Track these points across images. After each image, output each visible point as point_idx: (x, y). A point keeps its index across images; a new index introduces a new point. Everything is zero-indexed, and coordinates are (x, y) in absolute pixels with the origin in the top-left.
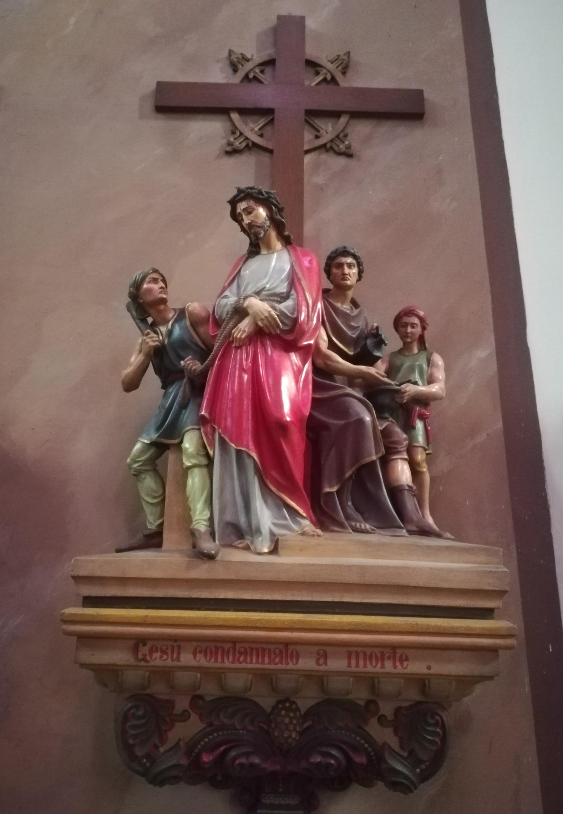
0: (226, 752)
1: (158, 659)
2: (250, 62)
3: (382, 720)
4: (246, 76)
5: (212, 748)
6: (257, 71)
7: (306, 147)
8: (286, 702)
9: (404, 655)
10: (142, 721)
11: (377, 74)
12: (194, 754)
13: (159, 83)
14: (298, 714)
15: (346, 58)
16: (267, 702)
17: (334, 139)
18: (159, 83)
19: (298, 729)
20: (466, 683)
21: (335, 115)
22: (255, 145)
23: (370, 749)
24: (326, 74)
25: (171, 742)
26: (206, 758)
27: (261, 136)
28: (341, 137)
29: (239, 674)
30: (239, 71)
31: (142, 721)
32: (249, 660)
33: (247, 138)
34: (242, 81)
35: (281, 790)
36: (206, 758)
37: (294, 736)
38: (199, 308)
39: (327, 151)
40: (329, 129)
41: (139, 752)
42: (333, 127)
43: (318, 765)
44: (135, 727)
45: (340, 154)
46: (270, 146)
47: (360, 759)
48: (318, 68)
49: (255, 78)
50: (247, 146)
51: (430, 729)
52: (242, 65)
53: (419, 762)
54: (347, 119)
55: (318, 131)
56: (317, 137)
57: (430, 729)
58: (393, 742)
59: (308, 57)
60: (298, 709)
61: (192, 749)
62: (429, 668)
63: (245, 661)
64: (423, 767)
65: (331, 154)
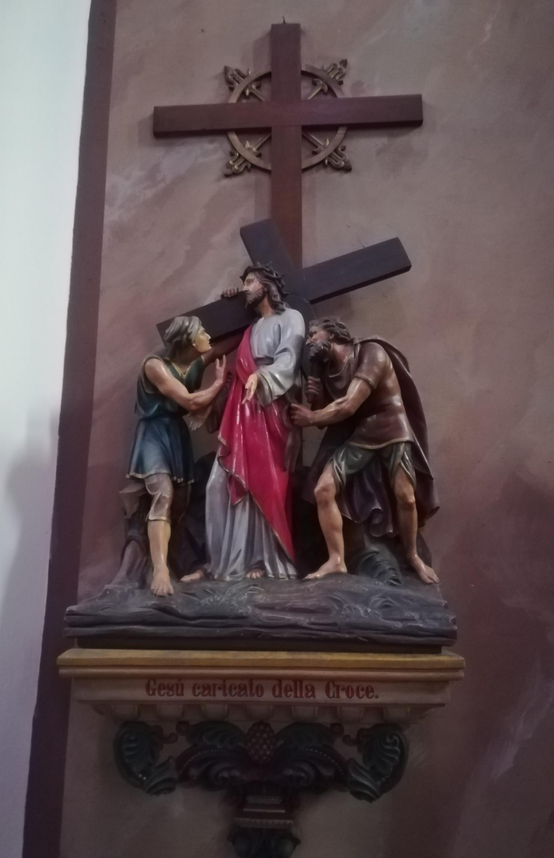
1: (166, 695)
2: (246, 79)
3: (346, 739)
4: (243, 93)
6: (254, 86)
7: (304, 166)
8: (262, 725)
11: (375, 80)
13: (156, 109)
16: (245, 726)
18: (156, 109)
21: (332, 128)
22: (254, 167)
24: (323, 85)
27: (259, 156)
28: (338, 151)
29: (216, 702)
30: (235, 90)
31: (134, 745)
32: (212, 693)
33: (246, 160)
37: (268, 753)
39: (325, 166)
40: (326, 144)
42: (330, 142)
45: (338, 169)
47: (327, 773)
48: (316, 80)
50: (246, 167)
51: (388, 747)
52: (238, 82)
56: (315, 153)
57: (388, 747)
58: (359, 758)
59: (304, 69)
63: (209, 694)
64: (384, 779)
65: (329, 169)
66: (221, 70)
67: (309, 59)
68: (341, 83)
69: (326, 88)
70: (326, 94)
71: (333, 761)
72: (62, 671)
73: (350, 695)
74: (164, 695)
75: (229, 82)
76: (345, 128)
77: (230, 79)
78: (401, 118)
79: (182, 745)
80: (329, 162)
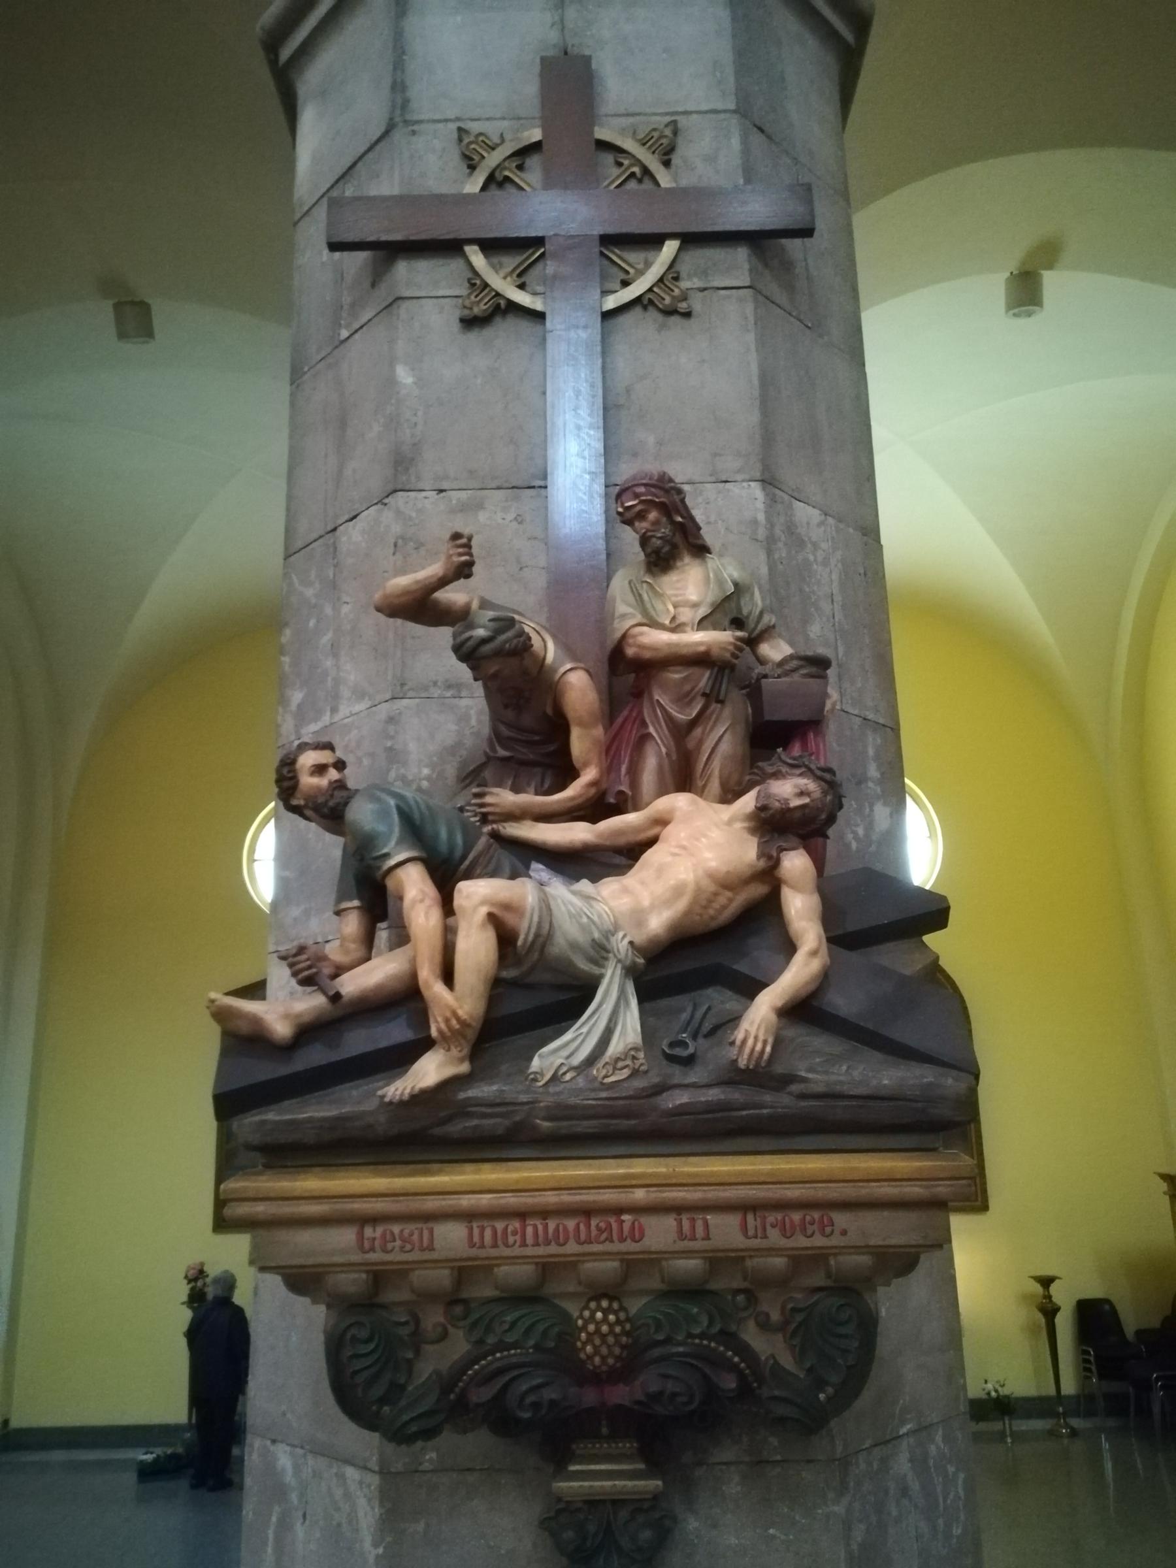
3: (765, 1325)
10: (372, 1346)
12: (457, 1390)
15: (668, 132)
31: (372, 1346)
34: (484, 188)
35: (605, 1431)
38: (574, 1446)
46: (537, 304)
47: (729, 1383)
49: (507, 179)
73: (788, 1234)
74: (812, 1236)
79: (459, 1345)
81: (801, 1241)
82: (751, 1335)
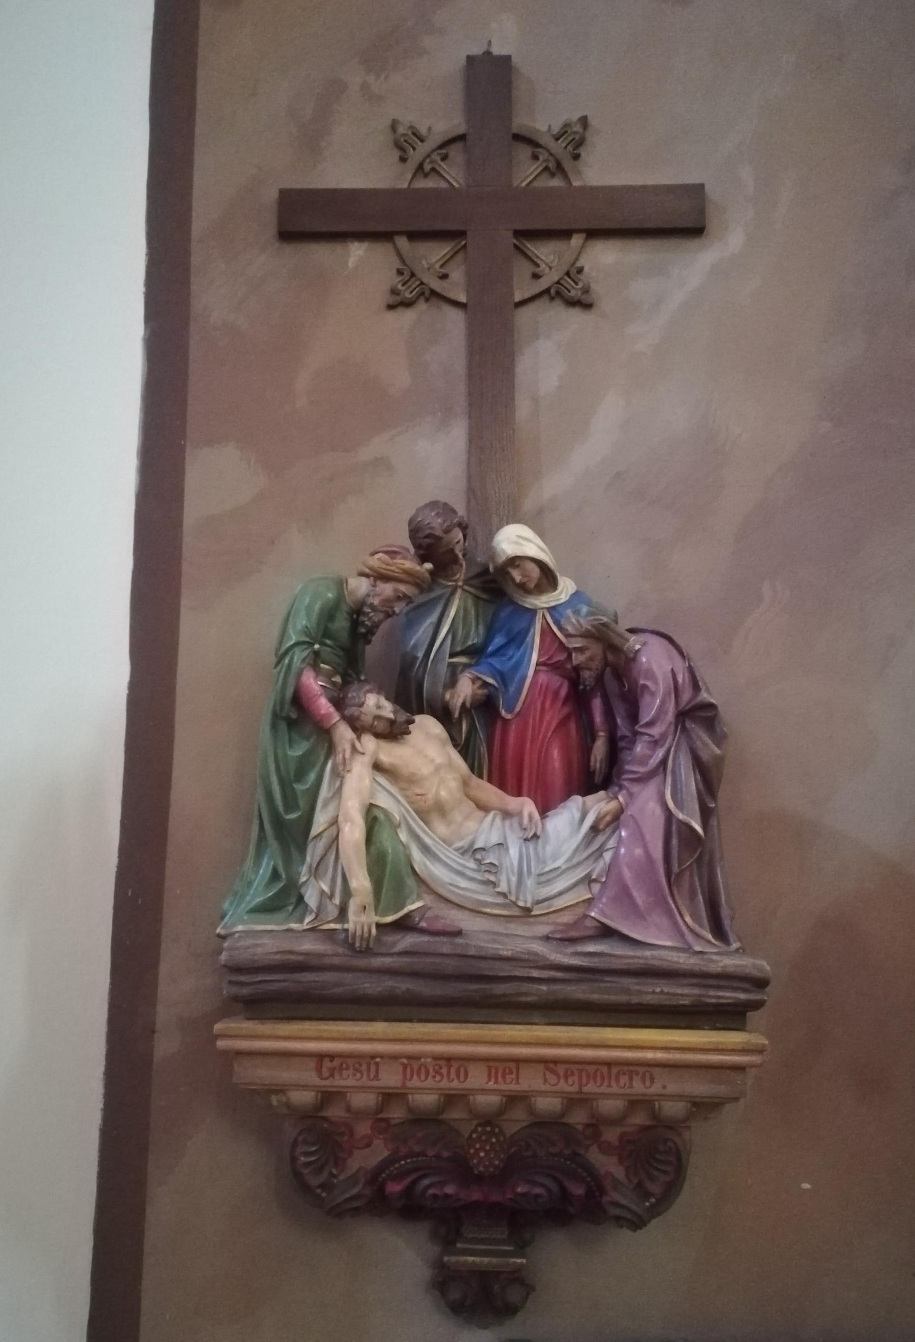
0: (414, 1183)
3: (606, 1148)
4: (420, 167)
5: (400, 1176)
6: (436, 157)
7: (518, 298)
9: (598, 1084)
14: (502, 1138)
17: (562, 278)
19: (502, 1156)
20: (704, 1107)
21: (565, 234)
22: (433, 293)
23: (589, 1179)
25: (349, 1172)
26: (394, 1188)
30: (409, 161)
33: (422, 283)
36: (394, 1188)
39: (552, 299)
41: (314, 1181)
43: (523, 1195)
44: (307, 1154)
47: (578, 1190)
52: (414, 149)
53: (647, 1195)
54: (581, 241)
55: (538, 266)
56: (536, 276)
58: (618, 1172)
60: (501, 1132)
61: (376, 1178)
62: (664, 1087)
66: (388, 122)
67: (544, 118)
68: (576, 157)
69: (552, 165)
70: (553, 175)
71: (585, 1174)
72: (221, 1044)
75: (398, 146)
76: (584, 235)
77: (403, 142)
78: (679, 220)
79: (380, 1152)
80: (558, 293)
81: (444, 1084)
82: (596, 1158)
